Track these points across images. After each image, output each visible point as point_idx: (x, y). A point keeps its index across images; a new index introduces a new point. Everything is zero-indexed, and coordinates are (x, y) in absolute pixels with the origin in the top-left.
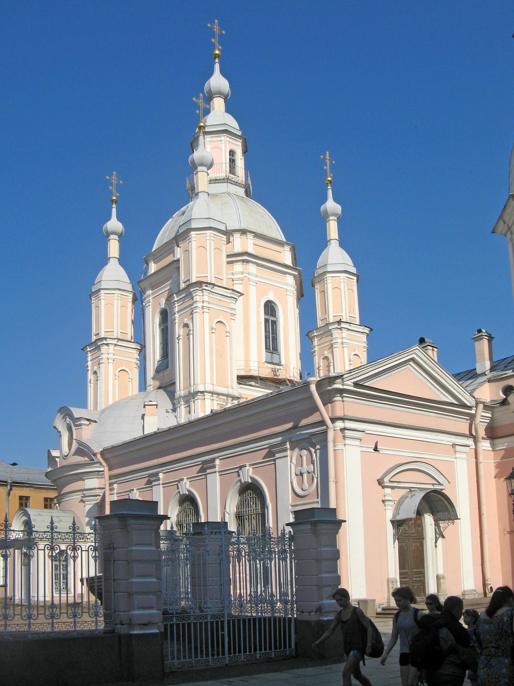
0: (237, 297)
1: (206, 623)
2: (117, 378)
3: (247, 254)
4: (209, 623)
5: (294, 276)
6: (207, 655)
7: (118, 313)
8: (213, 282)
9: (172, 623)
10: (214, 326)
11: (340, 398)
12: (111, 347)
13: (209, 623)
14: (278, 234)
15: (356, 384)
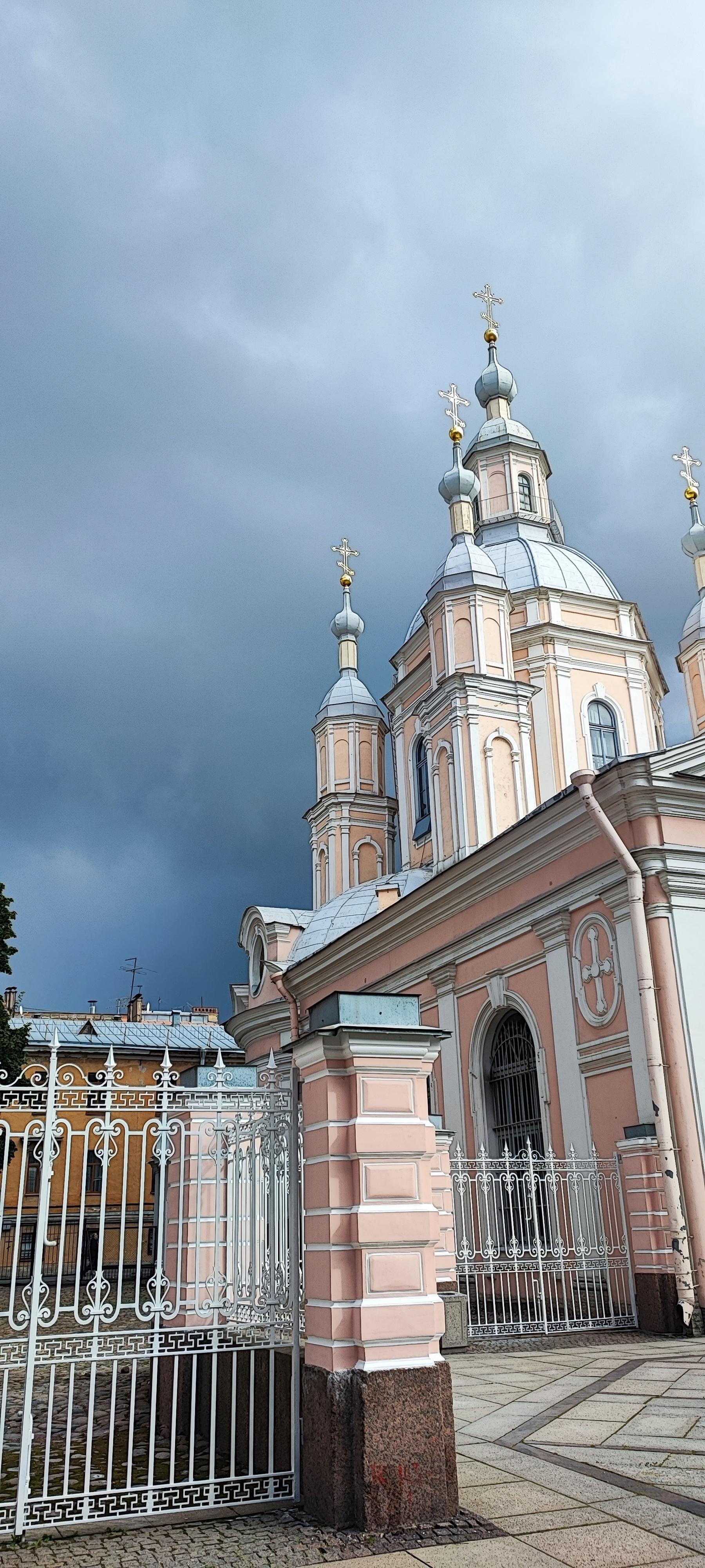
0: (530, 695)
1: (205, 1360)
2: (356, 857)
3: (549, 624)
4: (215, 1357)
5: (642, 655)
6: (563, 1318)
7: (685, 807)
8: (483, 672)
9: (205, 1351)
10: (489, 745)
11: (647, 809)
12: (346, 809)
13: (215, 1357)
14: (601, 588)
15: (680, 776)
